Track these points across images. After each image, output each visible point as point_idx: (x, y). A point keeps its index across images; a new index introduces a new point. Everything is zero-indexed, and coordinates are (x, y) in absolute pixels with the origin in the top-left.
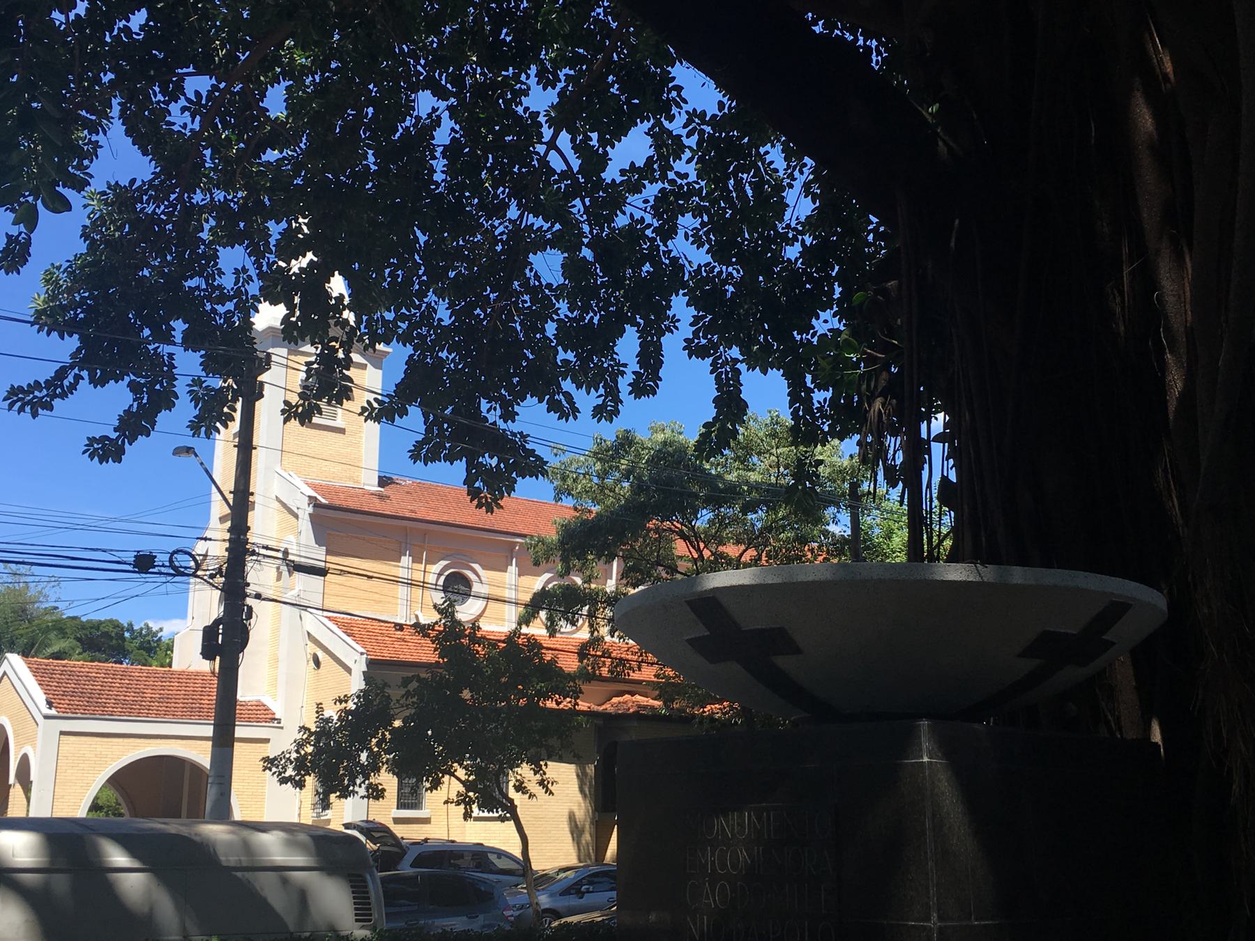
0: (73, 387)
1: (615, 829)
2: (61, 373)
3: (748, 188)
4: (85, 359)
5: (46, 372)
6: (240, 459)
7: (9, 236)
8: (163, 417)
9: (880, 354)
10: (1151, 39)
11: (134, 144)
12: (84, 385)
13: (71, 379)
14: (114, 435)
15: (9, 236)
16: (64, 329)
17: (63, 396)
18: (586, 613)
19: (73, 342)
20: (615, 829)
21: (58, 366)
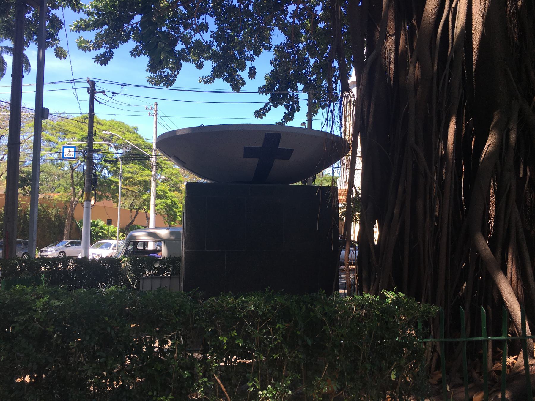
0: (270, 109)
1: (202, 180)
2: (266, 105)
3: (197, 289)
4: (272, 99)
5: (262, 106)
6: (359, 95)
7: (258, 57)
8: (296, 114)
9: (475, 142)
10: (431, 57)
11: (281, 32)
12: (272, 108)
13: (269, 106)
14: (281, 122)
15: (258, 57)
16: (266, 92)
17: (268, 111)
18: (344, 290)
19: (269, 95)
20: (202, 180)
21: (265, 103)
